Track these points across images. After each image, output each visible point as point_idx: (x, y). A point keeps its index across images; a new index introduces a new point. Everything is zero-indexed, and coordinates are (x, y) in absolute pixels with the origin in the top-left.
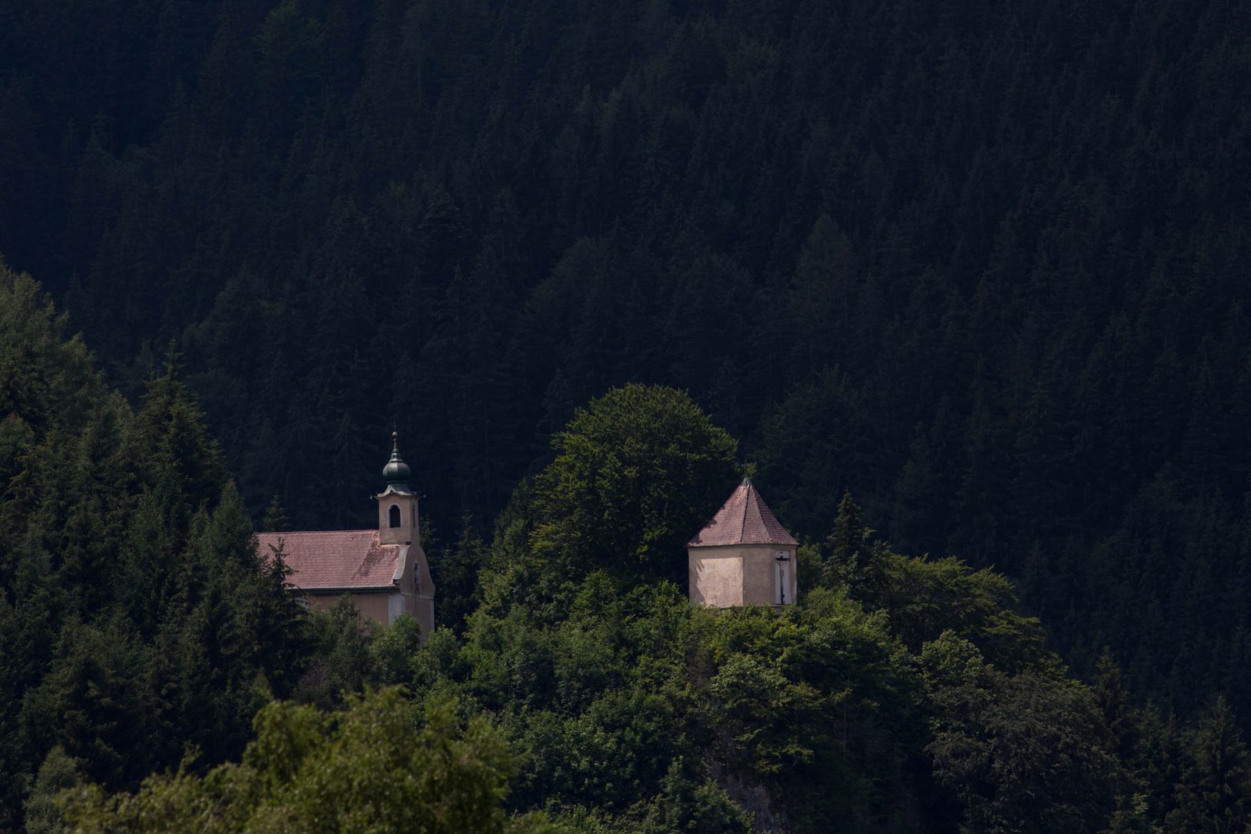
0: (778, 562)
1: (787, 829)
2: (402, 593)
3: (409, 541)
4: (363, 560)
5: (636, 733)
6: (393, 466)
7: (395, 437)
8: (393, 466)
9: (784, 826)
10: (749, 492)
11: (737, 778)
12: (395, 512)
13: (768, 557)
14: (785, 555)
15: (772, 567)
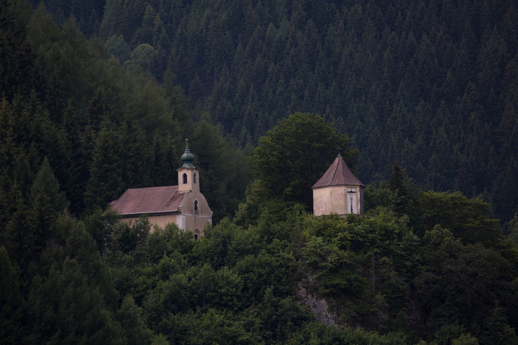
0: (350, 193)
1: (336, 320)
2: (182, 214)
3: (191, 190)
4: (169, 200)
5: (255, 275)
6: (185, 155)
7: (187, 141)
8: (185, 155)
9: (334, 319)
10: (339, 160)
11: (313, 296)
12: (185, 176)
13: (343, 191)
14: (353, 190)
15: (346, 197)
